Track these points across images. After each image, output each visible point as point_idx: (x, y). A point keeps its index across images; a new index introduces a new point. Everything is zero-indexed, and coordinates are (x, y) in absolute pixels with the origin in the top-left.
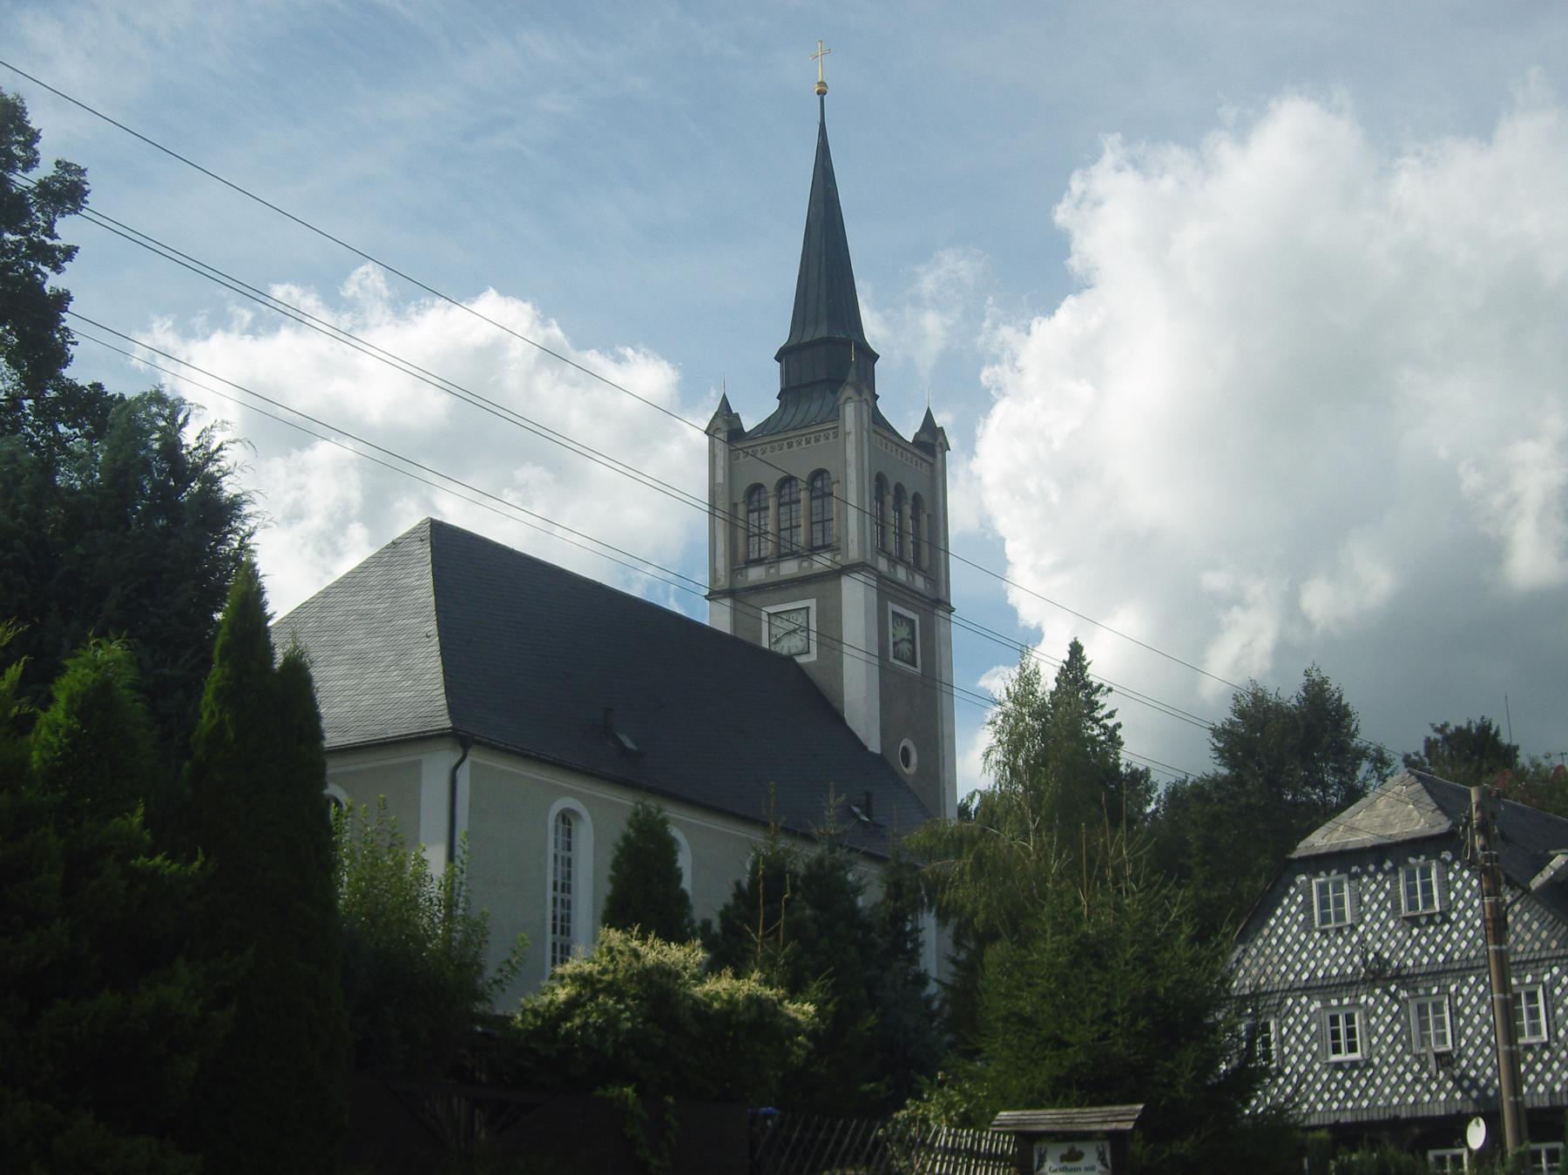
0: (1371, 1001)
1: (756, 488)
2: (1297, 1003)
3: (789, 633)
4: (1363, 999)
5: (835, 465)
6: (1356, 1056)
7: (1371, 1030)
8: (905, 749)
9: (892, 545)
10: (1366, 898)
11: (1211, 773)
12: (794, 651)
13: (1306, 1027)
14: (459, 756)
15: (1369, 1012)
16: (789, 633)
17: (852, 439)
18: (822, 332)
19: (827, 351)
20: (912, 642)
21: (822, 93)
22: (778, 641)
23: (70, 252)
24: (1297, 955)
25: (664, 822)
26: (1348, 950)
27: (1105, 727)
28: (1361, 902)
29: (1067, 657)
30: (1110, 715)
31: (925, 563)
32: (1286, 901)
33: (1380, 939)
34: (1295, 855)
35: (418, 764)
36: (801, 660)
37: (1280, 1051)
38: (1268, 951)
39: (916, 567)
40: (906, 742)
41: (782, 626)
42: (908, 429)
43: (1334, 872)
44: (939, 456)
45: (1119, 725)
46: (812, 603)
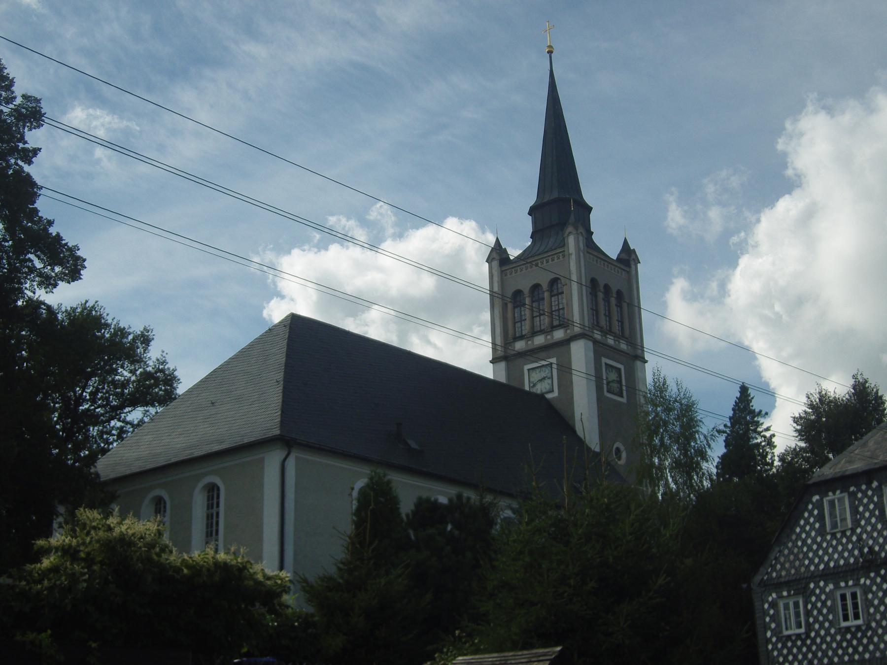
0: (868, 582)
1: (518, 293)
2: (817, 586)
3: (541, 380)
4: (862, 581)
5: (568, 276)
6: (860, 622)
7: (868, 603)
8: (618, 450)
9: (603, 321)
10: (861, 509)
11: (793, 446)
12: (544, 391)
13: (824, 603)
14: (286, 453)
15: (866, 590)
16: (541, 380)
17: (573, 257)
18: (555, 195)
19: (560, 204)
20: (620, 382)
21: (550, 52)
22: (534, 385)
23: (36, 151)
24: (816, 553)
25: (389, 482)
26: (850, 546)
27: (765, 437)
28: (857, 512)
29: (738, 395)
30: (768, 429)
31: (627, 333)
32: (806, 515)
33: (872, 537)
34: (811, 482)
35: (262, 460)
36: (549, 396)
37: (807, 621)
38: (796, 550)
39: (621, 336)
40: (617, 445)
41: (536, 376)
42: (613, 251)
43: (838, 492)
44: (633, 267)
45: (774, 435)
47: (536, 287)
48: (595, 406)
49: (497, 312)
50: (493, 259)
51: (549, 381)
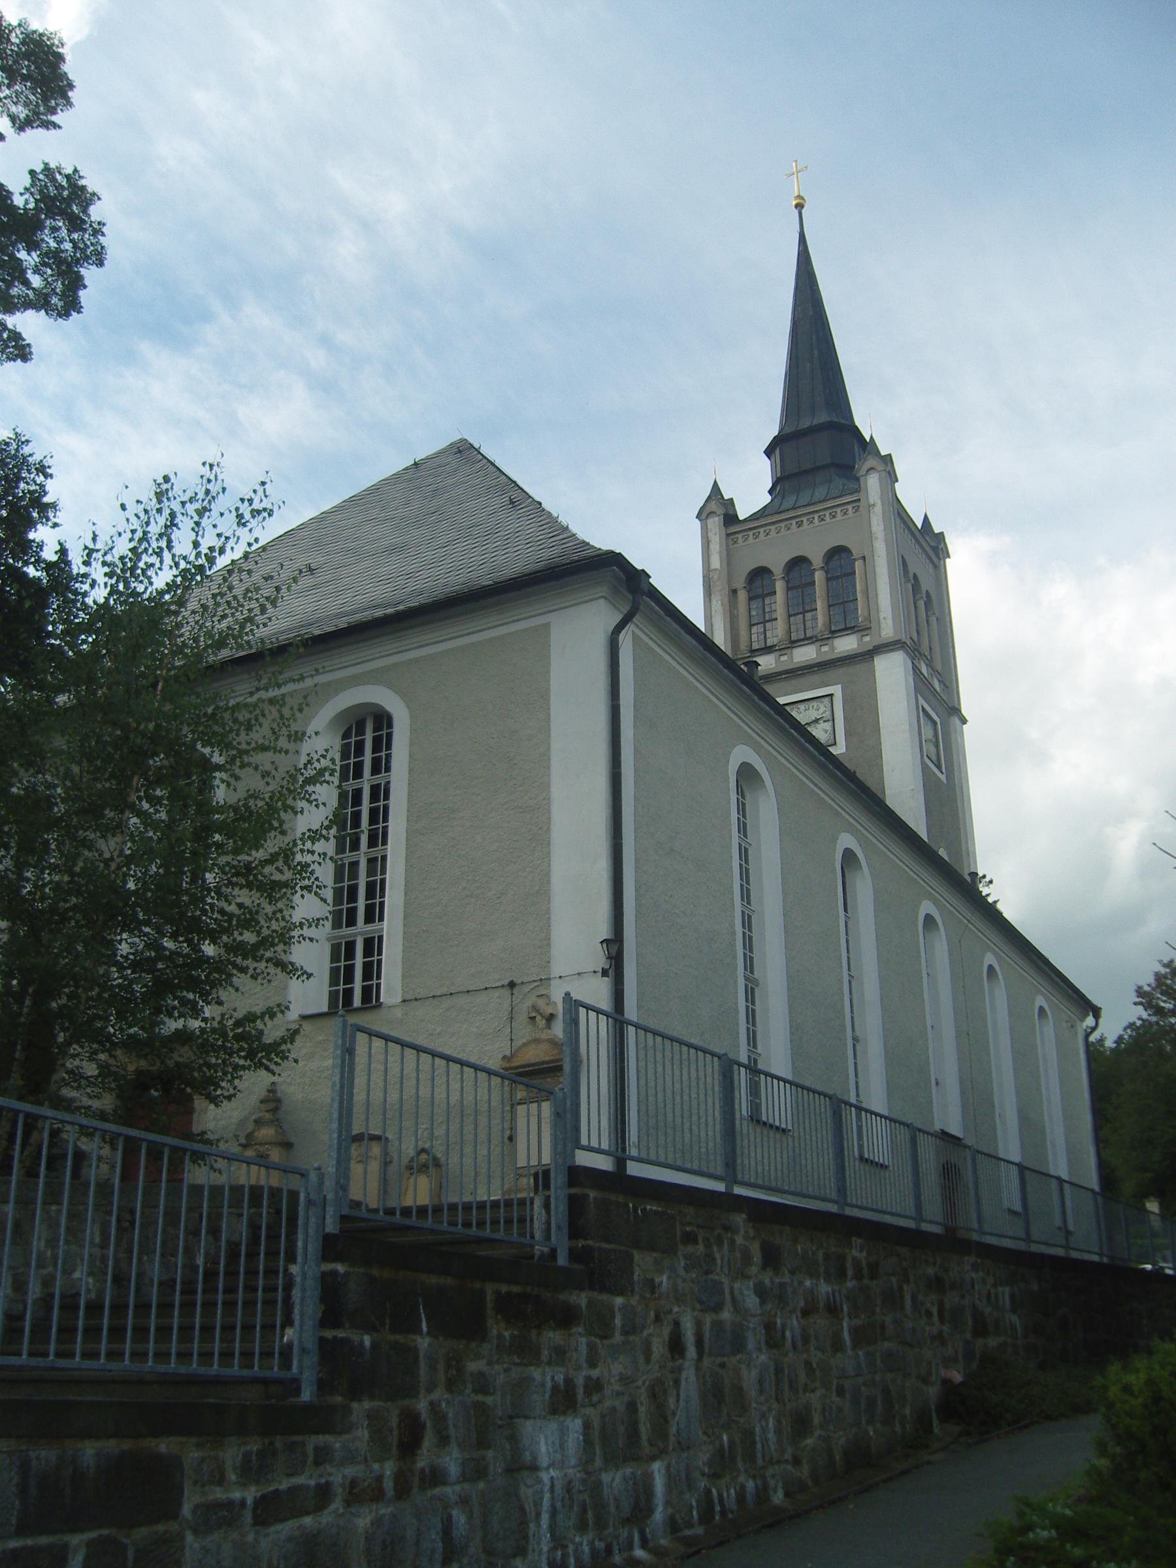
1: (760, 574)
21: (799, 206)
35: (547, 626)
46: (837, 690)
47: (798, 563)
49: (717, 605)
50: (712, 513)
51: (828, 726)
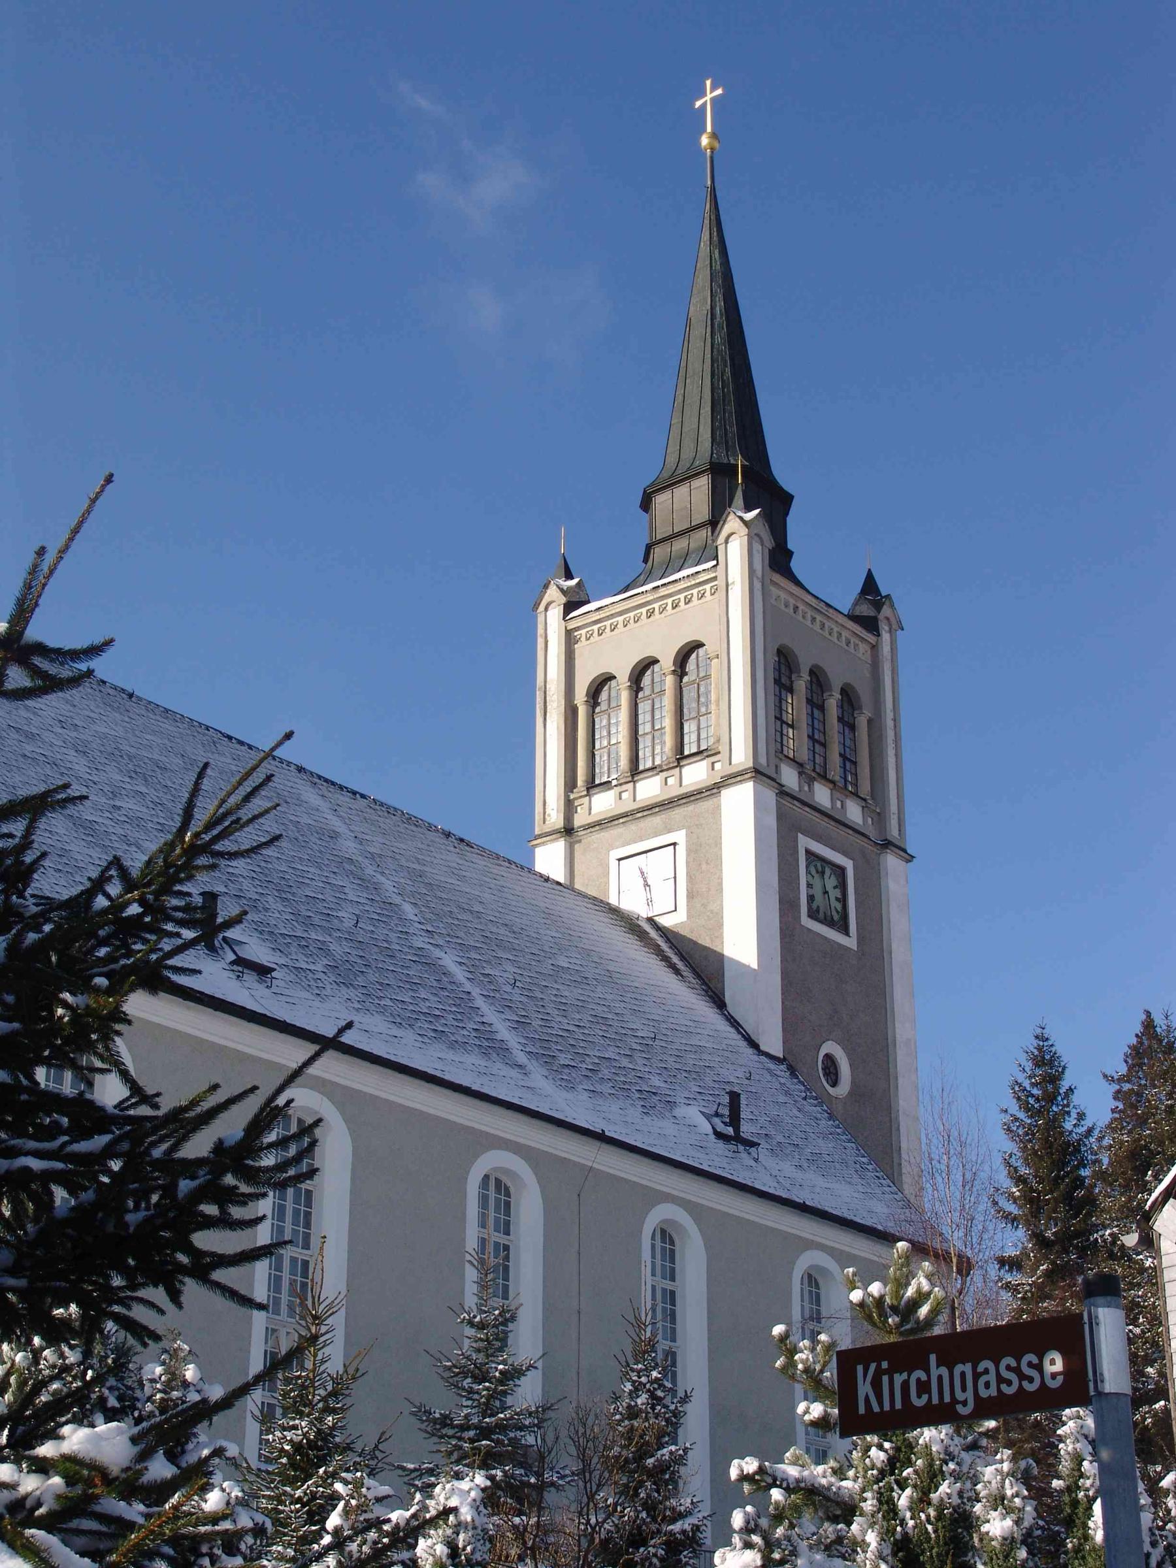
8: (829, 1057)
39: (846, 787)
40: (830, 1047)
46: (680, 836)
48: (777, 943)
